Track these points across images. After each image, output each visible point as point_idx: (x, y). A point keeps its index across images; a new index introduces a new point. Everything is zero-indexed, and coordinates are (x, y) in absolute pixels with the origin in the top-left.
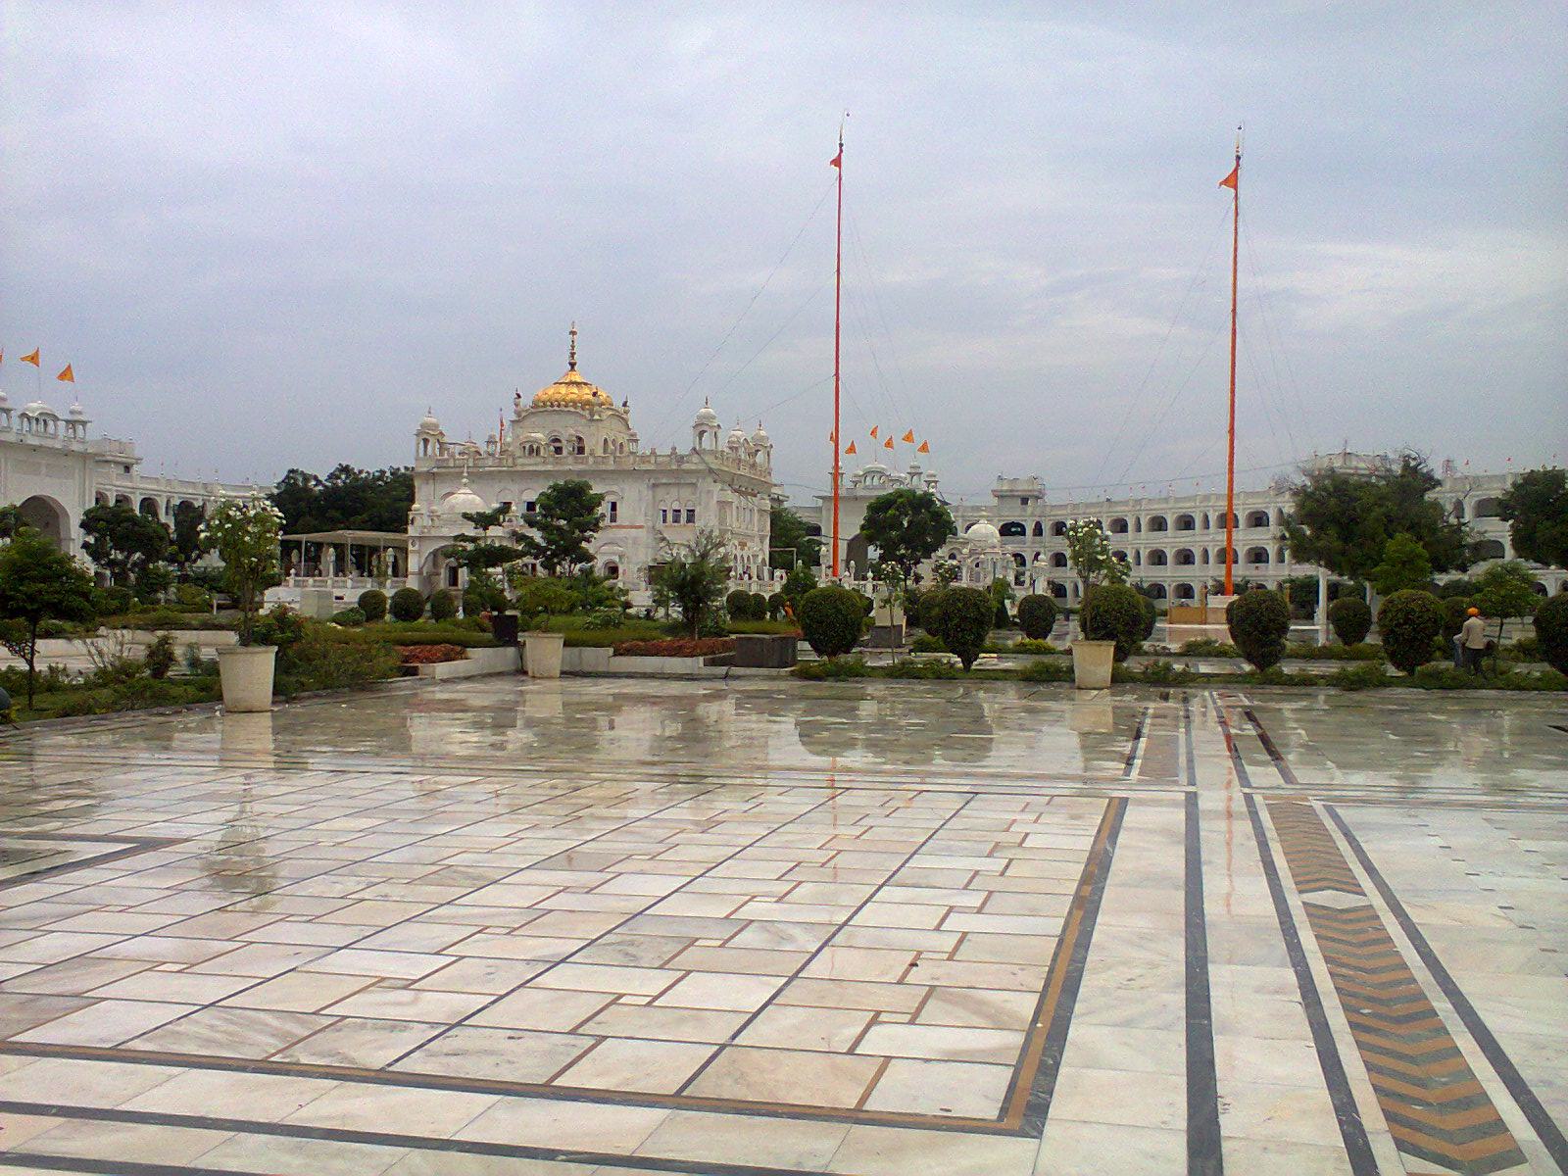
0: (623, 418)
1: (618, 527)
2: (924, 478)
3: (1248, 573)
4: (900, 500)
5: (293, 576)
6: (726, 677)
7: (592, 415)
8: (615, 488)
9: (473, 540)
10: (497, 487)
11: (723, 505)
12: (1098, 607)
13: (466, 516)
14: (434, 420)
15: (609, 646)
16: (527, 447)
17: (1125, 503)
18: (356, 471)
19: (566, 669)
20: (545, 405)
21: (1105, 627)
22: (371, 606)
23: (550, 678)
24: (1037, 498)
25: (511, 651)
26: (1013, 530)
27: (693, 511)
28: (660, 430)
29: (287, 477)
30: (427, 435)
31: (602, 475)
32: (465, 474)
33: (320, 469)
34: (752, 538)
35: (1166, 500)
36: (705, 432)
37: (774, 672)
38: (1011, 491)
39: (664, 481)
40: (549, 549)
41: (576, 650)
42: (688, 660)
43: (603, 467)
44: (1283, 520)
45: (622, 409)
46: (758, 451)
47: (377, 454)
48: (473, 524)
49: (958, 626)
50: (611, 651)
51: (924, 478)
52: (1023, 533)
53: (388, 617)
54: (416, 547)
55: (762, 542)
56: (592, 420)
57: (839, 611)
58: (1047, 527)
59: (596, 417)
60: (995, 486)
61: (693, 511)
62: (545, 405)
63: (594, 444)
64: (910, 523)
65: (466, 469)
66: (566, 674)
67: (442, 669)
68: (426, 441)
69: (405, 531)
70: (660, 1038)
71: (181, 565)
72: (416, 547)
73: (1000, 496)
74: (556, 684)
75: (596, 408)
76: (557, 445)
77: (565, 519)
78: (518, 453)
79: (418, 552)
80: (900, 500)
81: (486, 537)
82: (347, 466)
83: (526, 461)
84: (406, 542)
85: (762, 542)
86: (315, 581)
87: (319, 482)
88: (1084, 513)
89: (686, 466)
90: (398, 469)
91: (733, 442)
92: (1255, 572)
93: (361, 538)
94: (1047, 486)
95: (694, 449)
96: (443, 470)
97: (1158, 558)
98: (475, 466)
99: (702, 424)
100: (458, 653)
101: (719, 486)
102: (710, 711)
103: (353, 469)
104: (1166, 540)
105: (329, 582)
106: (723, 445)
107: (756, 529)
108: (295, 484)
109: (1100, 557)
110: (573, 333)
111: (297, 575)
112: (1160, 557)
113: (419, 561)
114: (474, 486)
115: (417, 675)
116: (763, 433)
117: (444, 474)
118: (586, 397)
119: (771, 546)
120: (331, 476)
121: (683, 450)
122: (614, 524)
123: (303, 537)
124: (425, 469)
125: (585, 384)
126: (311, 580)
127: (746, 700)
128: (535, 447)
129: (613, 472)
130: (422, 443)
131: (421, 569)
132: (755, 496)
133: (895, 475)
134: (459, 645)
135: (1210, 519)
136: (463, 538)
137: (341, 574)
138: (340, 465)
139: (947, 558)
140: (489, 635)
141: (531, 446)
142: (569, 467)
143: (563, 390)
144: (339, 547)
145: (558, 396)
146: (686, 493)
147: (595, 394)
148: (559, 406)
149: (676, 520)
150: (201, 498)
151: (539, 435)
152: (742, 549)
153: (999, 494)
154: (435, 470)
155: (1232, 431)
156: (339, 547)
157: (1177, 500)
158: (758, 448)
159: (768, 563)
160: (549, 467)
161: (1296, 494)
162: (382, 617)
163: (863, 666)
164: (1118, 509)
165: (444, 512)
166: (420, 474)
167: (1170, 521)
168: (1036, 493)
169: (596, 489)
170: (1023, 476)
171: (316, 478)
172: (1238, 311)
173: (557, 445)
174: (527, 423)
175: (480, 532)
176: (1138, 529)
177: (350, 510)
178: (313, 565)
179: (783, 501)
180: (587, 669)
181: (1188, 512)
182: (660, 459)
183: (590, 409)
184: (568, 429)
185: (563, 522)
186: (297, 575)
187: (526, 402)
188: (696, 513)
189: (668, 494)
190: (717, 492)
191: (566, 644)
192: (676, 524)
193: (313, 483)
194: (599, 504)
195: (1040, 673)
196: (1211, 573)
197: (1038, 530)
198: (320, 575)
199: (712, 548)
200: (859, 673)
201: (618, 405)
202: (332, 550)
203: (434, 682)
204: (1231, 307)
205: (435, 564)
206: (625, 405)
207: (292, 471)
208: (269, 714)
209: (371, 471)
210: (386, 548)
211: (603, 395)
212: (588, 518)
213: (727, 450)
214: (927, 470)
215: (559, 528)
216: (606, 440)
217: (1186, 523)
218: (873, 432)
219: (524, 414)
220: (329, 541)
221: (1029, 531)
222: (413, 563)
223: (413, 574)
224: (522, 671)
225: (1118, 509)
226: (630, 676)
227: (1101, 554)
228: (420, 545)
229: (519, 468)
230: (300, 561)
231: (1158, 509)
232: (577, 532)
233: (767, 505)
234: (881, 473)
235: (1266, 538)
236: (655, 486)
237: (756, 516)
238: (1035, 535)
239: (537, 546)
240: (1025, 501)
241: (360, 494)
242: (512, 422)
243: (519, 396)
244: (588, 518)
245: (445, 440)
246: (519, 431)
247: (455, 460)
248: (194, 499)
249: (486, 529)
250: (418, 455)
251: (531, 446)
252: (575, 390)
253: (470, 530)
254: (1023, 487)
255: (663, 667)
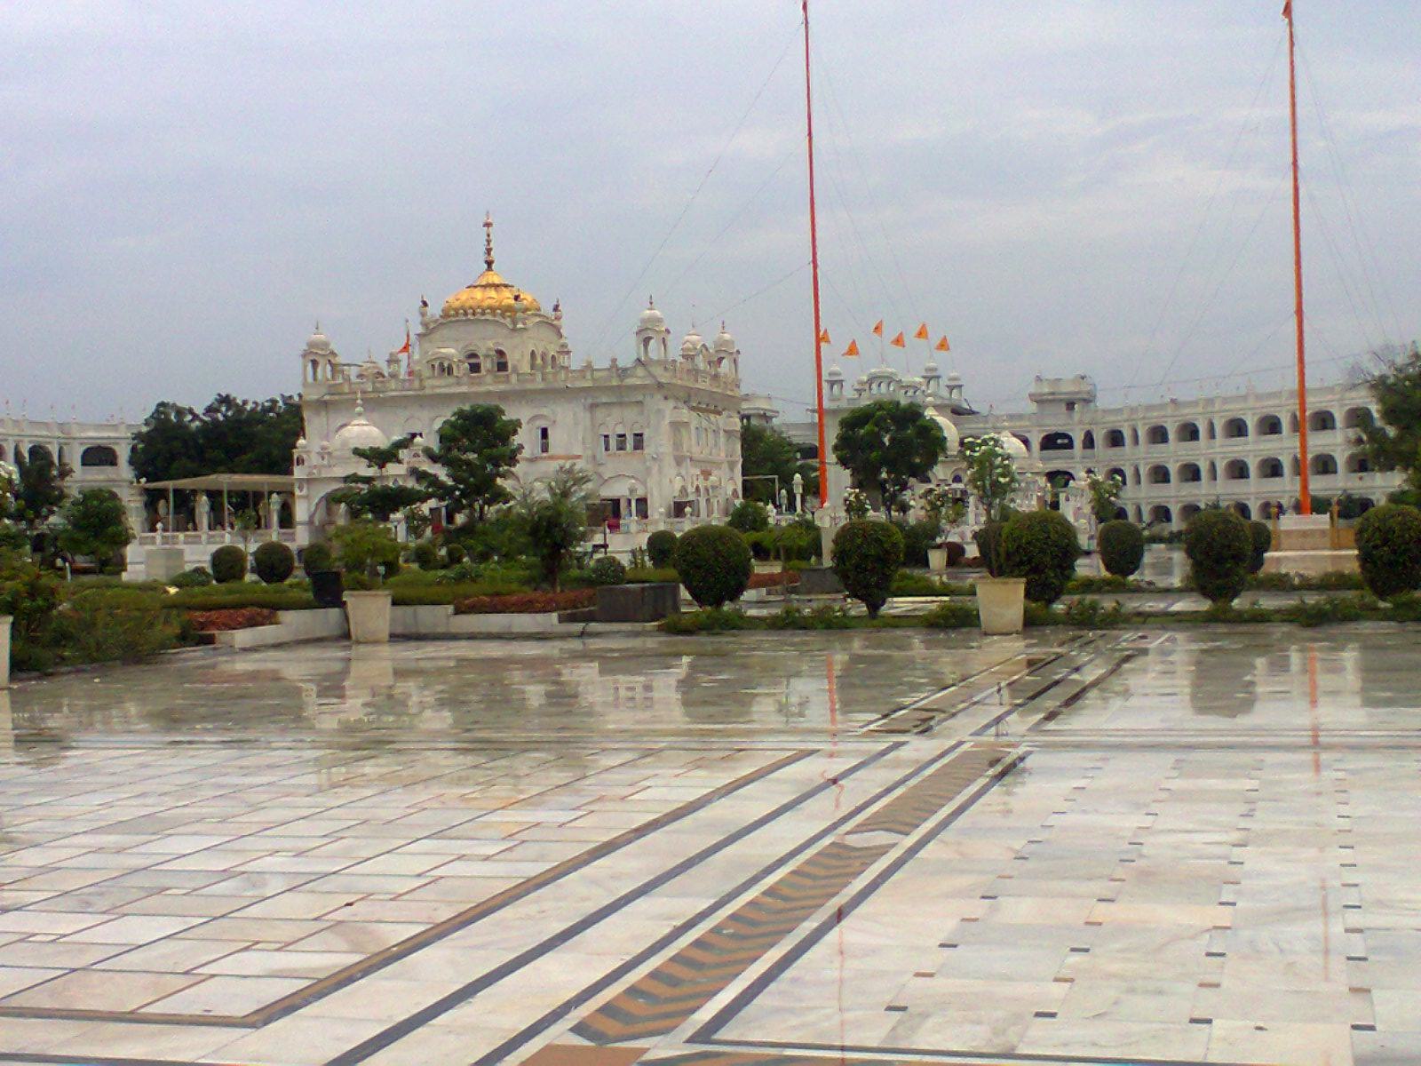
0: (552, 325)
1: (551, 458)
2: (944, 382)
3: (1349, 485)
4: (879, 413)
5: (159, 532)
6: (582, 635)
7: (514, 323)
8: (544, 411)
9: (368, 480)
10: (403, 414)
11: (677, 426)
12: (1020, 538)
13: (358, 452)
14: (322, 337)
15: (449, 603)
16: (437, 365)
17: (1195, 403)
18: (239, 401)
19: (399, 630)
20: (457, 314)
21: (1029, 561)
22: (226, 565)
23: (376, 642)
24: (1087, 401)
25: (334, 613)
26: (1059, 441)
27: (641, 435)
28: (597, 339)
29: (157, 411)
30: (315, 356)
31: (523, 396)
32: (359, 401)
33: (196, 398)
34: (718, 465)
35: (1245, 398)
36: (650, 338)
37: (638, 626)
38: (1053, 394)
39: (604, 401)
40: (459, 489)
41: (409, 610)
42: (540, 617)
43: (529, 386)
44: (1359, 417)
45: (551, 314)
46: (722, 359)
47: (261, 383)
48: (365, 462)
49: (857, 567)
50: (450, 608)
51: (944, 382)
52: (1070, 446)
53: (250, 577)
54: (305, 492)
55: (732, 470)
56: (514, 330)
57: (718, 552)
58: (1099, 437)
59: (520, 326)
60: (1033, 389)
61: (641, 435)
62: (457, 314)
63: (518, 358)
64: (892, 440)
65: (359, 395)
66: (395, 638)
67: (242, 637)
68: (315, 363)
69: (291, 473)
70: (750, 1039)
71: (31, 522)
72: (305, 492)
73: (1040, 400)
74: (386, 651)
75: (519, 315)
76: (473, 361)
77: (474, 452)
78: (427, 373)
79: (307, 497)
80: (879, 413)
81: (382, 477)
82: (228, 396)
83: (435, 382)
84: (292, 485)
85: (732, 470)
86: (186, 536)
87: (195, 417)
88: (1144, 418)
89: (629, 381)
90: (291, 397)
91: (689, 349)
92: (1358, 484)
93: (242, 483)
94: (1099, 388)
95: (639, 360)
96: (337, 397)
97: (1161, 475)
98: (375, 390)
99: (647, 329)
100: (265, 617)
101: (671, 403)
102: (570, 674)
103: (235, 399)
104: (1248, 448)
105: (204, 537)
106: (675, 353)
107: (723, 454)
108: (168, 419)
109: (1002, 480)
110: (488, 225)
111: (165, 530)
112: (1242, 469)
113: (309, 509)
114: (375, 416)
115: (213, 643)
116: (727, 336)
117: (334, 403)
118: (506, 302)
119: (743, 475)
120: (209, 410)
121: (625, 361)
122: (545, 455)
123: (170, 485)
124: (316, 397)
125: (506, 286)
126: (181, 536)
127: (609, 662)
128: (446, 365)
129: (542, 391)
130: (310, 365)
131: (312, 517)
132: (719, 413)
133: (907, 379)
134: (266, 608)
135: (1140, 433)
136: (355, 478)
137: (219, 527)
138: (219, 395)
139: (950, 482)
140: (310, 595)
141: (441, 364)
142: (488, 385)
143: (478, 294)
144: (214, 495)
145: (471, 303)
146: (630, 414)
147: (517, 298)
148: (474, 314)
149: (621, 447)
150: (55, 441)
151: (452, 351)
152: (706, 479)
153: (1039, 398)
154: (327, 397)
155: (1299, 312)
156: (214, 495)
157: (1259, 397)
158: (722, 355)
159: (741, 496)
160: (464, 389)
161: (1373, 387)
162: (241, 577)
163: (742, 617)
164: (1186, 411)
165: (335, 447)
166: (309, 403)
167: (1251, 423)
168: (1085, 396)
169: (510, 414)
170: (1068, 374)
171: (191, 411)
172: (1301, 163)
173: (473, 361)
174: (437, 336)
175: (371, 472)
176: (1212, 435)
177: (216, 451)
178: (185, 516)
179: (771, 418)
180: (423, 630)
181: (1272, 411)
182: (597, 375)
183: (512, 315)
184: (486, 342)
185: (472, 456)
186: (165, 530)
187: (435, 310)
188: (645, 437)
189: (609, 415)
190: (670, 411)
191: (395, 603)
192: (622, 452)
193: (189, 417)
194: (515, 432)
195: (946, 618)
196: (1253, 490)
197: (1089, 442)
198: (195, 529)
199: (574, 485)
200: (739, 624)
201: (547, 310)
202: (205, 498)
203: (231, 650)
204: (1291, 160)
205: (329, 511)
206: (556, 308)
207: (162, 404)
208: (6, 692)
209: (259, 401)
210: (270, 493)
211: (528, 299)
212: (501, 449)
213: (680, 359)
214: (947, 373)
215: (468, 463)
216: (533, 353)
217: (1190, 432)
218: (876, 328)
219: (432, 326)
220: (203, 487)
221: (1078, 443)
222: (301, 512)
223: (301, 524)
224: (346, 635)
225: (1186, 411)
226: (472, 637)
227: (1004, 475)
228: (308, 489)
229: (428, 391)
230: (168, 514)
231: (1235, 409)
232: (489, 467)
233: (736, 424)
234: (890, 379)
235: (1337, 443)
236: (593, 406)
237: (722, 439)
238: (1085, 447)
239: (442, 485)
240: (1070, 405)
241: (245, 429)
242: (419, 335)
243: (425, 304)
244: (501, 449)
245: (340, 360)
246: (426, 345)
247: (350, 383)
248: (49, 443)
249: (382, 466)
250: (305, 378)
251: (441, 364)
252: (492, 293)
253: (364, 470)
254: (1067, 388)
255: (510, 627)
